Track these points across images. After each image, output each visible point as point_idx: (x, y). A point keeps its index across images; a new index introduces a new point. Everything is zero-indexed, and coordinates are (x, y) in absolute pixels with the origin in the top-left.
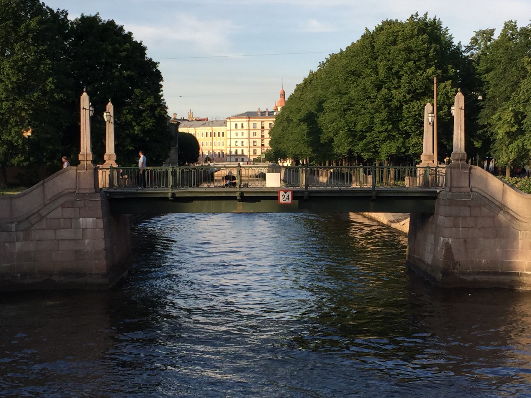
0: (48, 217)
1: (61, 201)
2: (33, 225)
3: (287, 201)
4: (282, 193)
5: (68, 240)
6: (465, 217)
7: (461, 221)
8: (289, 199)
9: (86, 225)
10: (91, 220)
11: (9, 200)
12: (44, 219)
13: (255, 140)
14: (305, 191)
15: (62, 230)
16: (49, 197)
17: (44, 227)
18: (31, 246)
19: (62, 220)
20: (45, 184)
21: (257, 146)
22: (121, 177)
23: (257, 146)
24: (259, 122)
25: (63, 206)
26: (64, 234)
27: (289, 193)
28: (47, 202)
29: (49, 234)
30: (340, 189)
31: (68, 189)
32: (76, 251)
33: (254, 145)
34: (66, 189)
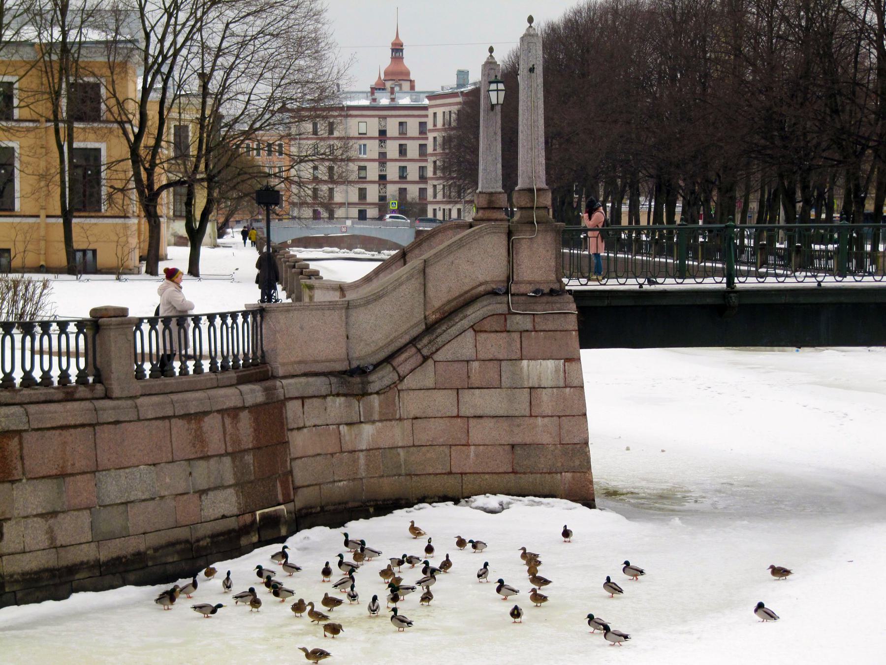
1: (474, 313)
2: (401, 379)
5: (494, 417)
9: (539, 378)
10: (550, 364)
11: (344, 311)
12: (430, 362)
13: (362, 164)
14: (729, 292)
15: (477, 391)
16: (437, 304)
17: (430, 383)
18: (397, 434)
19: (475, 365)
21: (368, 179)
22: (868, 248)
23: (368, 179)
24: (372, 119)
25: (476, 328)
29: (443, 401)
30: (819, 283)
31: (486, 283)
32: (513, 446)
33: (360, 178)
34: (481, 284)
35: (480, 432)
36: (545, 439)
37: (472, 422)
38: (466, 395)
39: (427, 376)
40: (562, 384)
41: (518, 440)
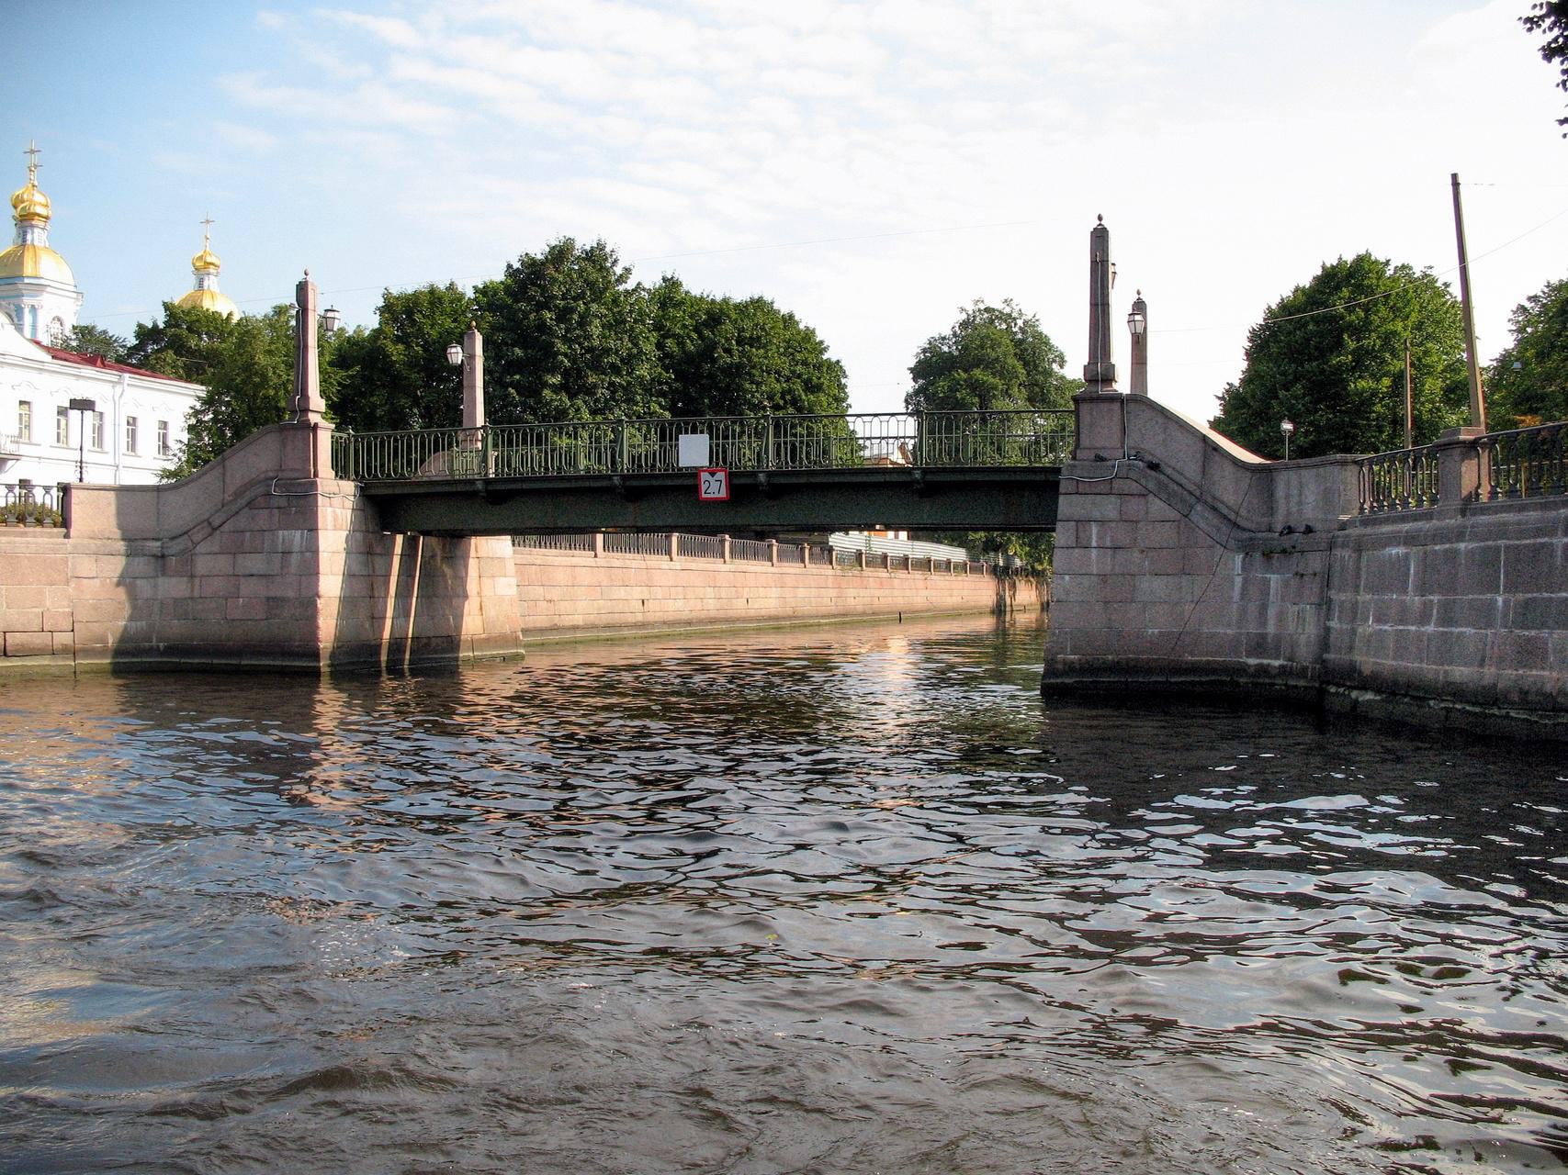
2: (195, 545)
6: (1101, 522)
7: (1094, 531)
16: (231, 489)
20: (228, 463)
26: (254, 563)
28: (228, 498)
29: (222, 563)
32: (268, 599)
35: (249, 588)
36: (290, 594)
37: (242, 580)
38: (240, 558)
40: (303, 549)
41: (272, 594)
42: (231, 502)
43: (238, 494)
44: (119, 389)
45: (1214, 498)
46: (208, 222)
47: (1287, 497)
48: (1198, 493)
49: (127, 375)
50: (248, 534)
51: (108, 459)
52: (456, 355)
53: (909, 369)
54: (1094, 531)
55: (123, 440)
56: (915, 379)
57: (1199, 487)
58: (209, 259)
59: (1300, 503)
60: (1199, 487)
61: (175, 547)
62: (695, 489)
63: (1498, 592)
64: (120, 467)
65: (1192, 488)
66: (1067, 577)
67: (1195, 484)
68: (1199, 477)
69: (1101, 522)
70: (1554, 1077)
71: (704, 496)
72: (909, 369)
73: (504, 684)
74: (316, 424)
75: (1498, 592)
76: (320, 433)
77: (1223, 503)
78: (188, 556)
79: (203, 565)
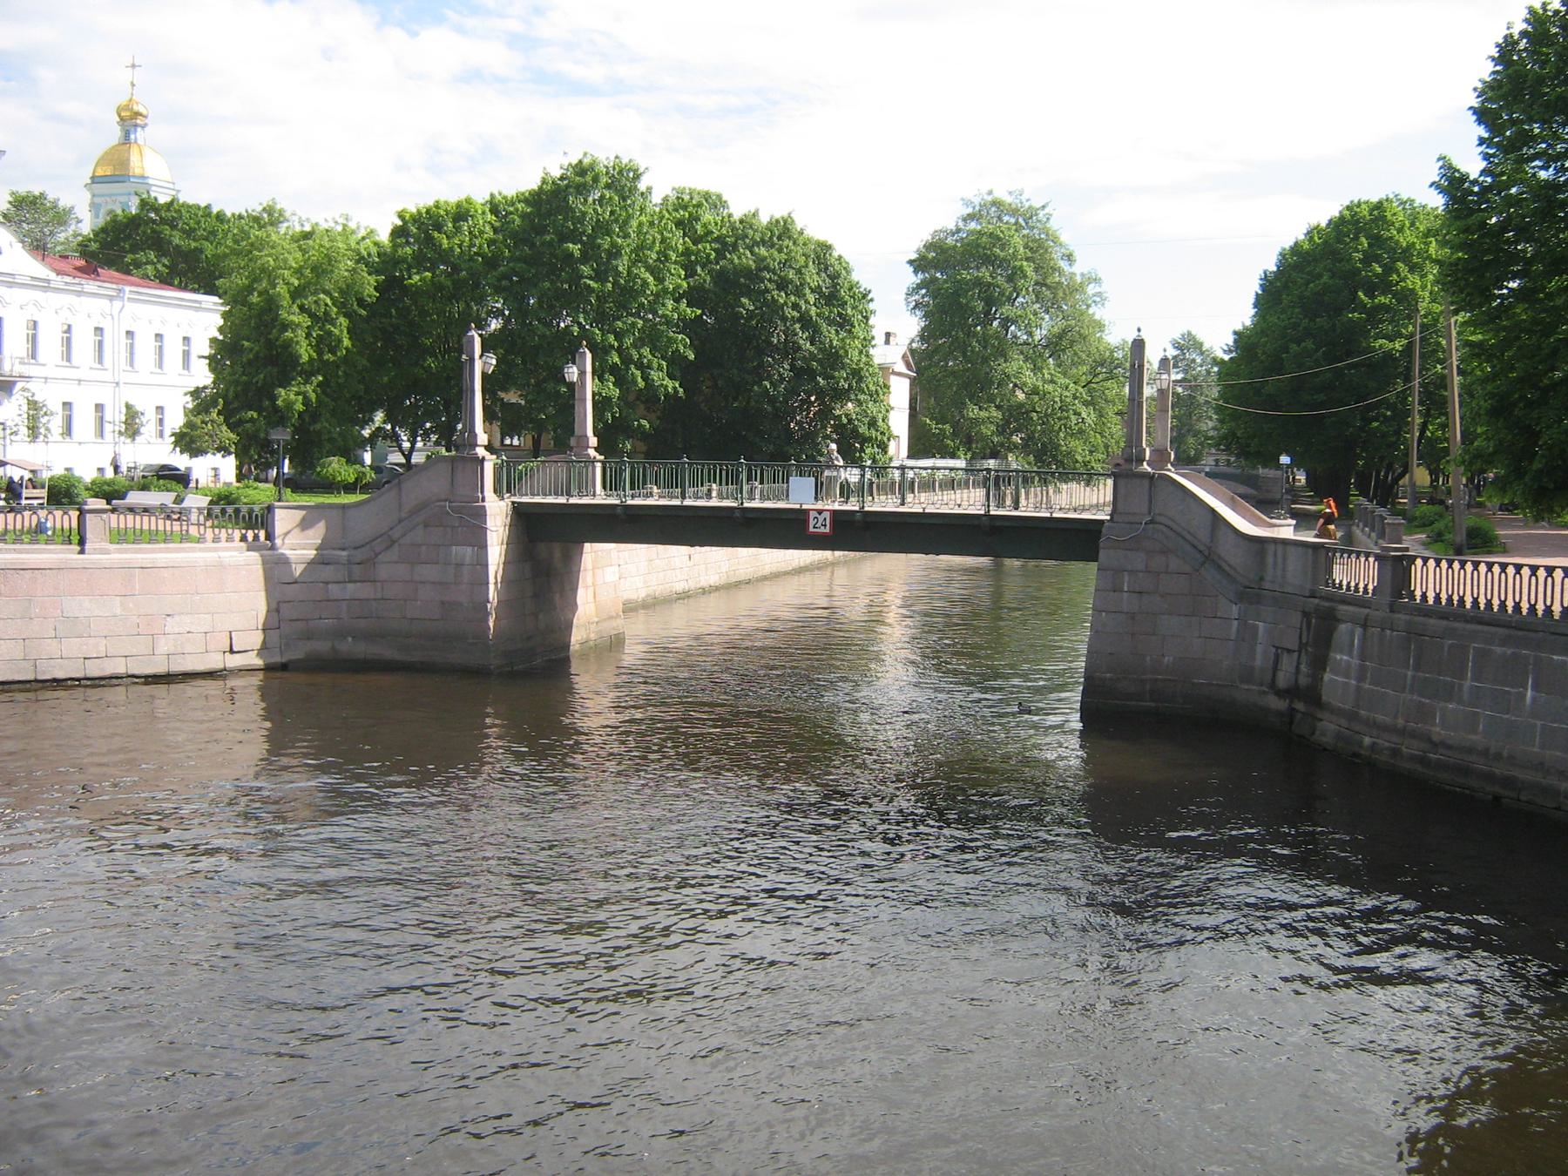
0: (401, 541)
2: (377, 555)
3: (822, 530)
4: (813, 514)
6: (1131, 572)
7: (1126, 579)
8: (825, 525)
10: (469, 549)
12: (397, 544)
26: (427, 572)
27: (827, 515)
32: (443, 603)
39: (393, 554)
42: (406, 518)
43: (414, 512)
44: (117, 304)
45: (1220, 557)
46: (133, 66)
47: (1275, 563)
48: (1206, 553)
49: (127, 289)
50: (424, 548)
51: (107, 376)
52: (572, 373)
53: (911, 262)
54: (1126, 579)
55: (124, 354)
56: (916, 272)
57: (1210, 548)
58: (136, 108)
59: (1284, 570)
60: (1210, 548)
61: (359, 555)
62: (806, 522)
63: (1408, 669)
64: (121, 385)
65: (1201, 548)
66: (1104, 614)
67: (1205, 545)
68: (1209, 540)
69: (1131, 572)
70: (146, 677)
71: (811, 529)
72: (911, 262)
73: (577, 655)
74: (483, 458)
75: (1408, 669)
76: (486, 464)
77: (1226, 562)
78: (370, 562)
79: (383, 572)
